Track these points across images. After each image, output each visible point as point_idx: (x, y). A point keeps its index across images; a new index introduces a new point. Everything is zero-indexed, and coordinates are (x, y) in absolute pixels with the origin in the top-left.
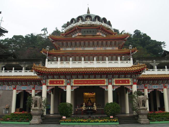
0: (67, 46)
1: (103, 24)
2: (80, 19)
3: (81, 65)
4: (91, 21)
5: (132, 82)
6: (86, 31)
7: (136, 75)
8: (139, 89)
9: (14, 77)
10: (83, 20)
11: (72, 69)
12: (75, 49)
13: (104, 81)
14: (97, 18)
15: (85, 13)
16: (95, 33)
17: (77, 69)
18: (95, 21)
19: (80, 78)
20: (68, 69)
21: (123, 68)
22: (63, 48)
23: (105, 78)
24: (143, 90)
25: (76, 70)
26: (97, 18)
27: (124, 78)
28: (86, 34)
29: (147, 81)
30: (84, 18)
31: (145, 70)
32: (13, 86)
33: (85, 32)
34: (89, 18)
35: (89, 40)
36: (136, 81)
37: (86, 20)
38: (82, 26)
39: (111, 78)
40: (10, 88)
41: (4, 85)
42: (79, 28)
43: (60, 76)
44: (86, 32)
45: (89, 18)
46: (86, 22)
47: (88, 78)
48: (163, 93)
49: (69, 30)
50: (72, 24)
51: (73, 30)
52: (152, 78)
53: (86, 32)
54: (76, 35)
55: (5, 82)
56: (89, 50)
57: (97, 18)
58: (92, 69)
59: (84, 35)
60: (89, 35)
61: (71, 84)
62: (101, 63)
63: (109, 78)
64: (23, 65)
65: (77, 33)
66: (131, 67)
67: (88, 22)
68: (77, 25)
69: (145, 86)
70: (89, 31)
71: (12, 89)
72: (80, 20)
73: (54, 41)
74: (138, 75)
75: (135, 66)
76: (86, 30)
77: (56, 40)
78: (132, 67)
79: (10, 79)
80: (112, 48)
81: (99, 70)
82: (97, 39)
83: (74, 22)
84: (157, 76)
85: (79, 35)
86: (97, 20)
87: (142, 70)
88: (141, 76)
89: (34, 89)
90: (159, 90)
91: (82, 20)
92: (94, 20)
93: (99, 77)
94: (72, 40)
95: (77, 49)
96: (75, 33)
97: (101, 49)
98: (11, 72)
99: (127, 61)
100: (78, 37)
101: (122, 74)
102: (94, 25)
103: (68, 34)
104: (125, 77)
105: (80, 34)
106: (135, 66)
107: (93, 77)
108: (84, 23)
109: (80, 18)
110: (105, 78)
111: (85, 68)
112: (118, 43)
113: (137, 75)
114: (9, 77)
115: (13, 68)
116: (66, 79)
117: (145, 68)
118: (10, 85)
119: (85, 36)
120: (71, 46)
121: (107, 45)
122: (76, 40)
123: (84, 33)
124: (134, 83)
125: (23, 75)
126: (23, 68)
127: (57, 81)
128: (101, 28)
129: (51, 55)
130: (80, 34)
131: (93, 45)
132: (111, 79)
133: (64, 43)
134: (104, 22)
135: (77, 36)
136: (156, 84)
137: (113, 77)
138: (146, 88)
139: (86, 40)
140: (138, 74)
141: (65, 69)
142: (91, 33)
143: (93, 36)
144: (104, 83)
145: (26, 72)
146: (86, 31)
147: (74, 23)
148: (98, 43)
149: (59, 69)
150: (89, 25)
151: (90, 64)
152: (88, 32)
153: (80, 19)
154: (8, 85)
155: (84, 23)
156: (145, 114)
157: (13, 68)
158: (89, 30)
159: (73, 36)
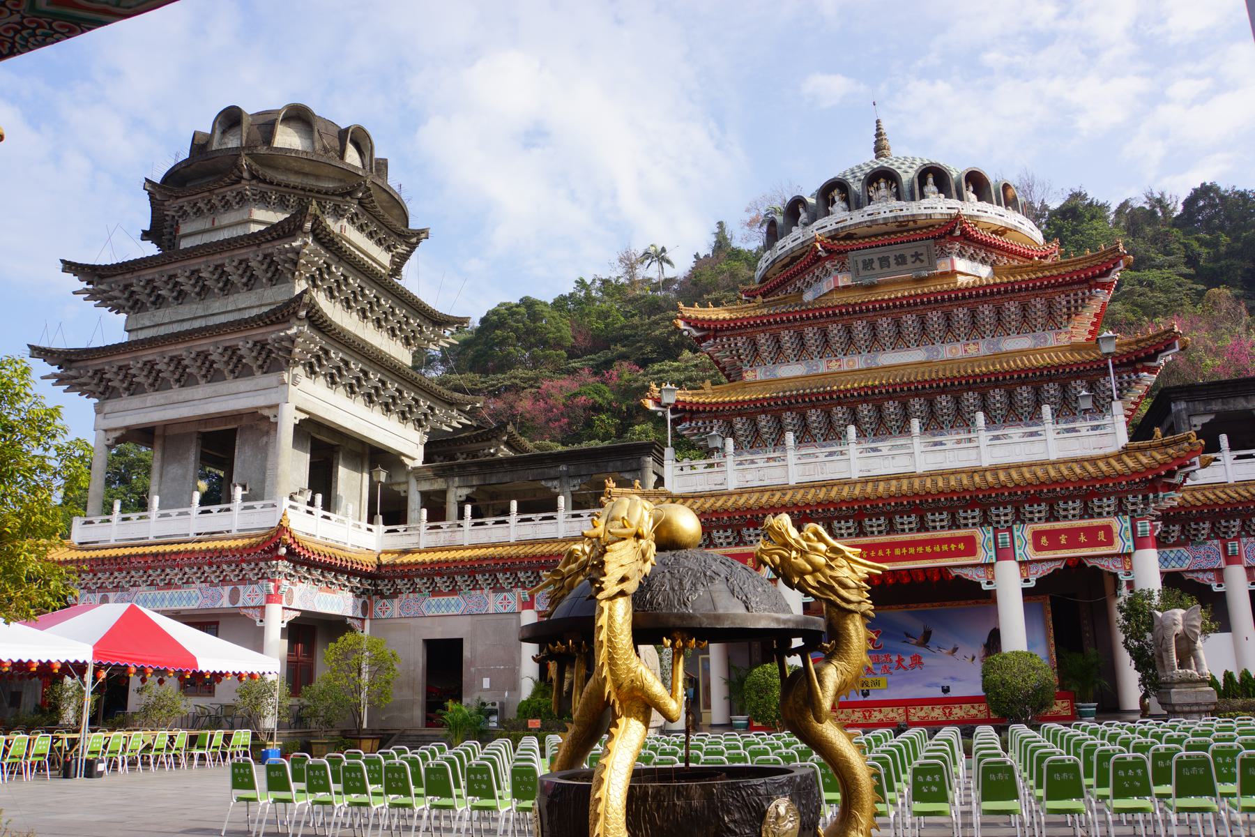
0: (778, 354)
1: (971, 206)
2: (837, 198)
3: (843, 464)
4: (899, 199)
5: (1129, 534)
6: (875, 257)
7: (1145, 498)
8: (1192, 571)
9: (522, 550)
10: (854, 203)
11: (802, 491)
12: (822, 367)
13: (1108, 529)
14: (931, 180)
15: (866, 159)
16: (926, 264)
17: (824, 489)
18: (923, 196)
19: (903, 530)
20: (778, 495)
21: (1086, 464)
22: (758, 370)
23: (974, 524)
24: (1219, 572)
25: (822, 494)
26: (934, 176)
27: (1081, 517)
28: (877, 276)
29: (1238, 522)
30: (856, 187)
31: (1194, 464)
32: (519, 590)
33: (868, 264)
34: (882, 185)
35: (895, 308)
36: (1155, 527)
37: (870, 199)
38: (850, 237)
39: (1006, 522)
40: (505, 603)
41: (478, 592)
42: (841, 246)
43: (739, 533)
44: (876, 265)
45: (882, 185)
46: (868, 209)
47: (888, 533)
48: (1223, 593)
49: (784, 266)
50: (797, 232)
51: (804, 263)
52: (1216, 504)
53: (876, 265)
54: (832, 284)
55: (479, 577)
56: (1018, 347)
57: (931, 180)
58: (905, 484)
59: (866, 281)
60: (895, 282)
61: (1018, 552)
62: (949, 445)
63: (998, 522)
64: (555, 483)
65: (828, 274)
66: (1118, 457)
67: (885, 208)
68: (643, 272)
69: (1225, 548)
70: (892, 261)
71: (514, 605)
72: (834, 202)
73: (704, 339)
74: (1161, 494)
75: (1139, 449)
76: (875, 254)
77: (716, 330)
78: (1126, 450)
79: (502, 558)
80: (1035, 338)
81: (953, 483)
82: (943, 299)
83: (803, 216)
84: (513, 551)
85: (841, 284)
86: (931, 188)
87: (1181, 467)
88: (1173, 499)
89: (532, 608)
90: (1195, 575)
91: (846, 200)
92: (917, 192)
93: (942, 520)
94: (802, 318)
95: (834, 366)
96: (818, 279)
97: (972, 350)
98: (552, 518)
99: (693, 462)
100: (838, 299)
101: (1034, 499)
102: (915, 222)
103: (782, 285)
104: (1087, 513)
105: (844, 280)
106: (1139, 449)
107: (942, 520)
108: (857, 217)
109: (834, 190)
110: (974, 524)
111: (865, 481)
112: (1069, 309)
113: (1156, 497)
114: (451, 555)
115: (514, 505)
116: (990, 524)
117: (1193, 453)
118: (502, 589)
119: (871, 287)
120: (802, 350)
121: (1001, 326)
122: (823, 316)
123: (862, 273)
124: (1139, 543)
125: (561, 537)
126: (561, 500)
127: (1073, 533)
128: (958, 233)
129: (698, 411)
130: (844, 280)
131: (924, 335)
132: (1010, 529)
133: (762, 339)
134: (973, 197)
135: (826, 290)
136: (1175, 544)
137: (1019, 518)
138: (1232, 559)
139: (957, 298)
140: (1156, 492)
141: (762, 491)
142: (905, 267)
143: (920, 280)
144: (1110, 542)
145: (574, 516)
146: (875, 257)
147: (806, 225)
148: (973, 314)
149: (731, 494)
150: (886, 222)
151: (893, 457)
152: (884, 262)
153: (836, 194)
154: (497, 589)
155: (857, 217)
156: (1195, 708)
157: (514, 505)
158: (892, 253)
159: (808, 296)
